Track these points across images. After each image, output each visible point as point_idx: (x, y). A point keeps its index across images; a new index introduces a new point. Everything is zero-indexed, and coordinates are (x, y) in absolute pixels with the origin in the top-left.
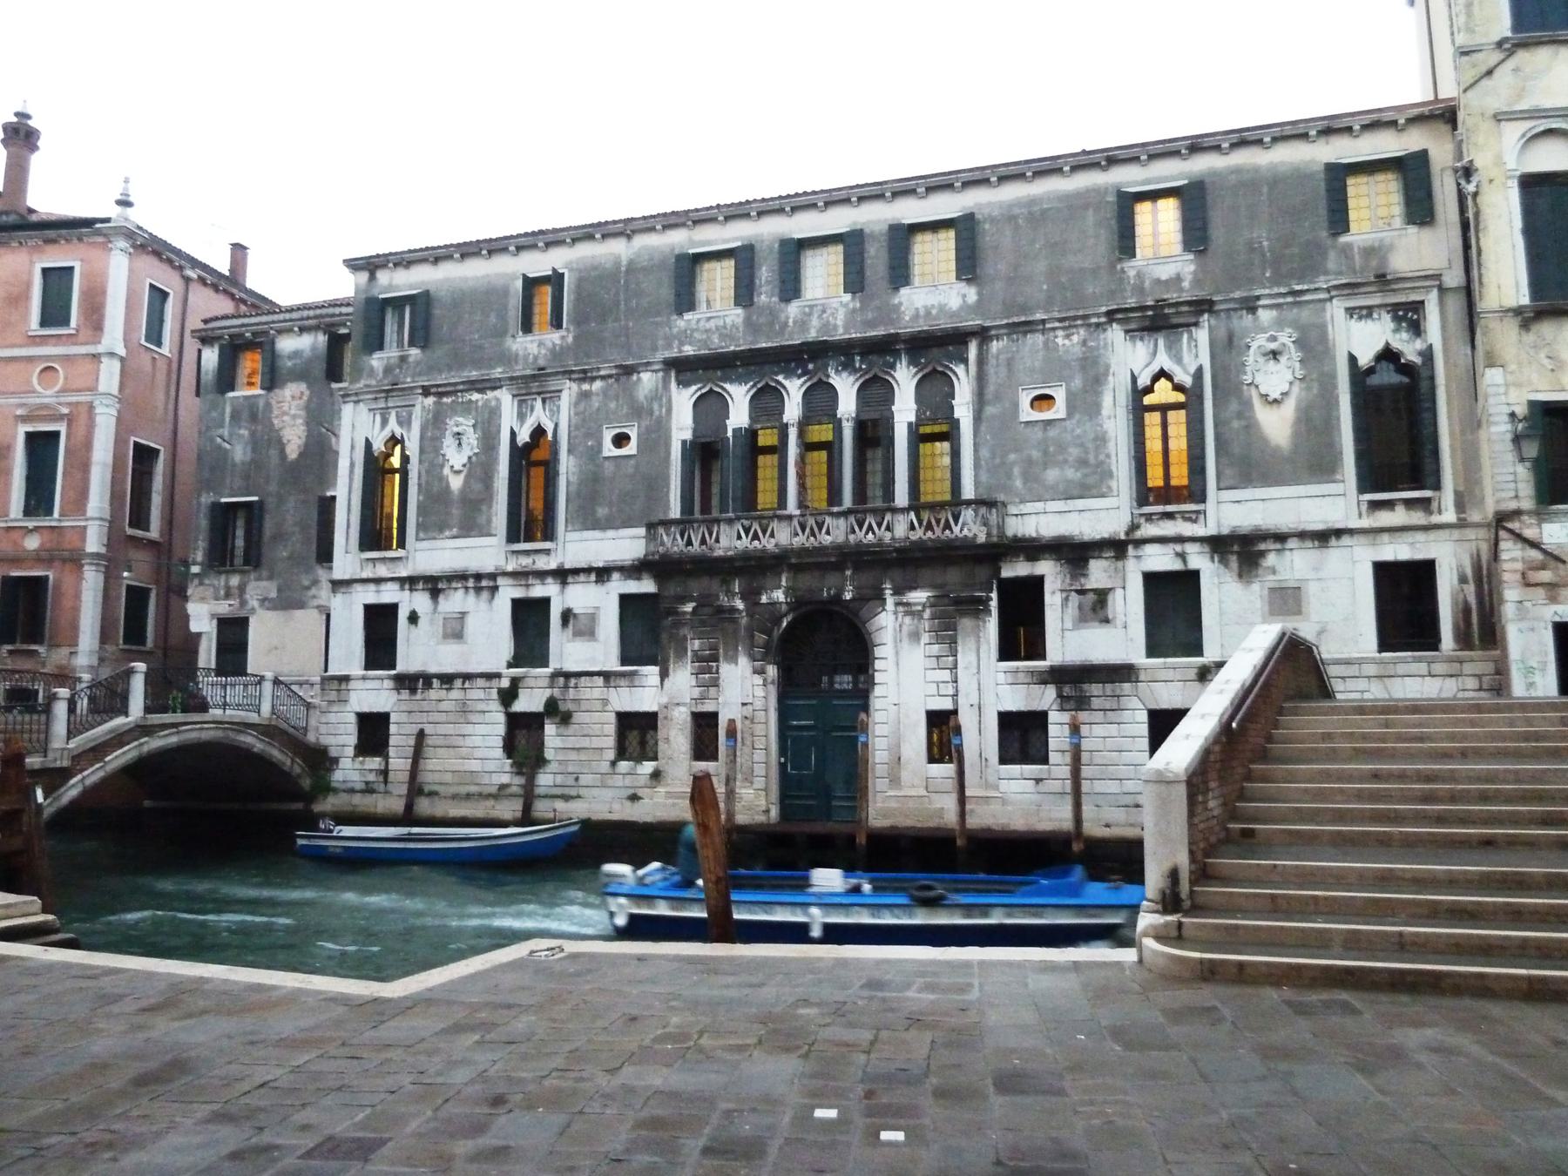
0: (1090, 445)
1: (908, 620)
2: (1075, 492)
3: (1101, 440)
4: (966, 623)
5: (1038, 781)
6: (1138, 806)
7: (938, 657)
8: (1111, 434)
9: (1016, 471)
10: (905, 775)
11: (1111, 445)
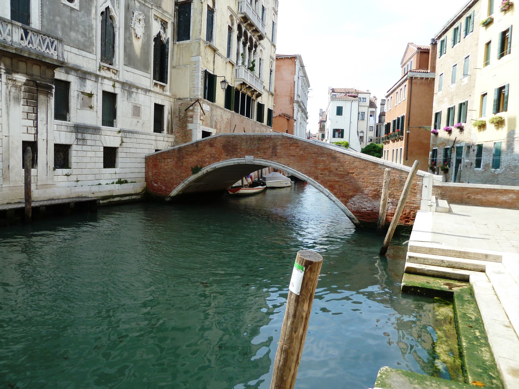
0: (87, 28)
1: (13, 90)
2: (81, 47)
3: (91, 27)
4: (42, 98)
5: (67, 175)
6: (100, 184)
7: (28, 113)
8: (94, 26)
9: (59, 26)
10: (12, 175)
11: (94, 31)
